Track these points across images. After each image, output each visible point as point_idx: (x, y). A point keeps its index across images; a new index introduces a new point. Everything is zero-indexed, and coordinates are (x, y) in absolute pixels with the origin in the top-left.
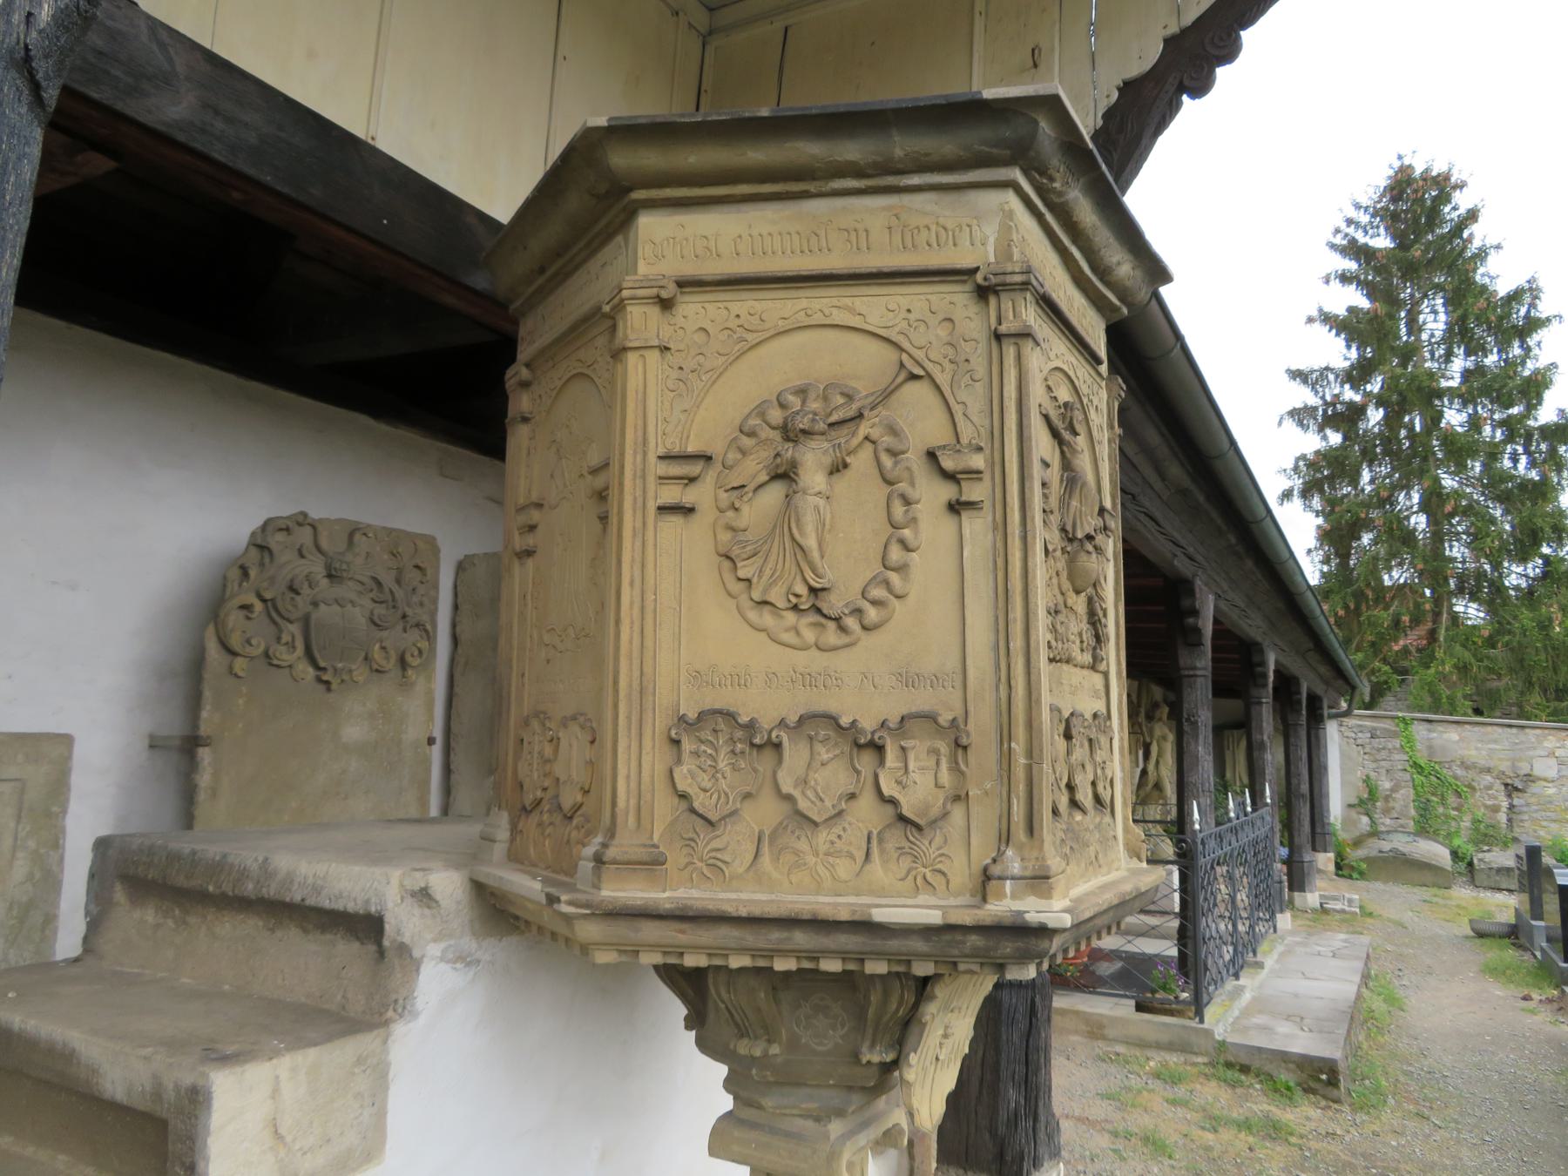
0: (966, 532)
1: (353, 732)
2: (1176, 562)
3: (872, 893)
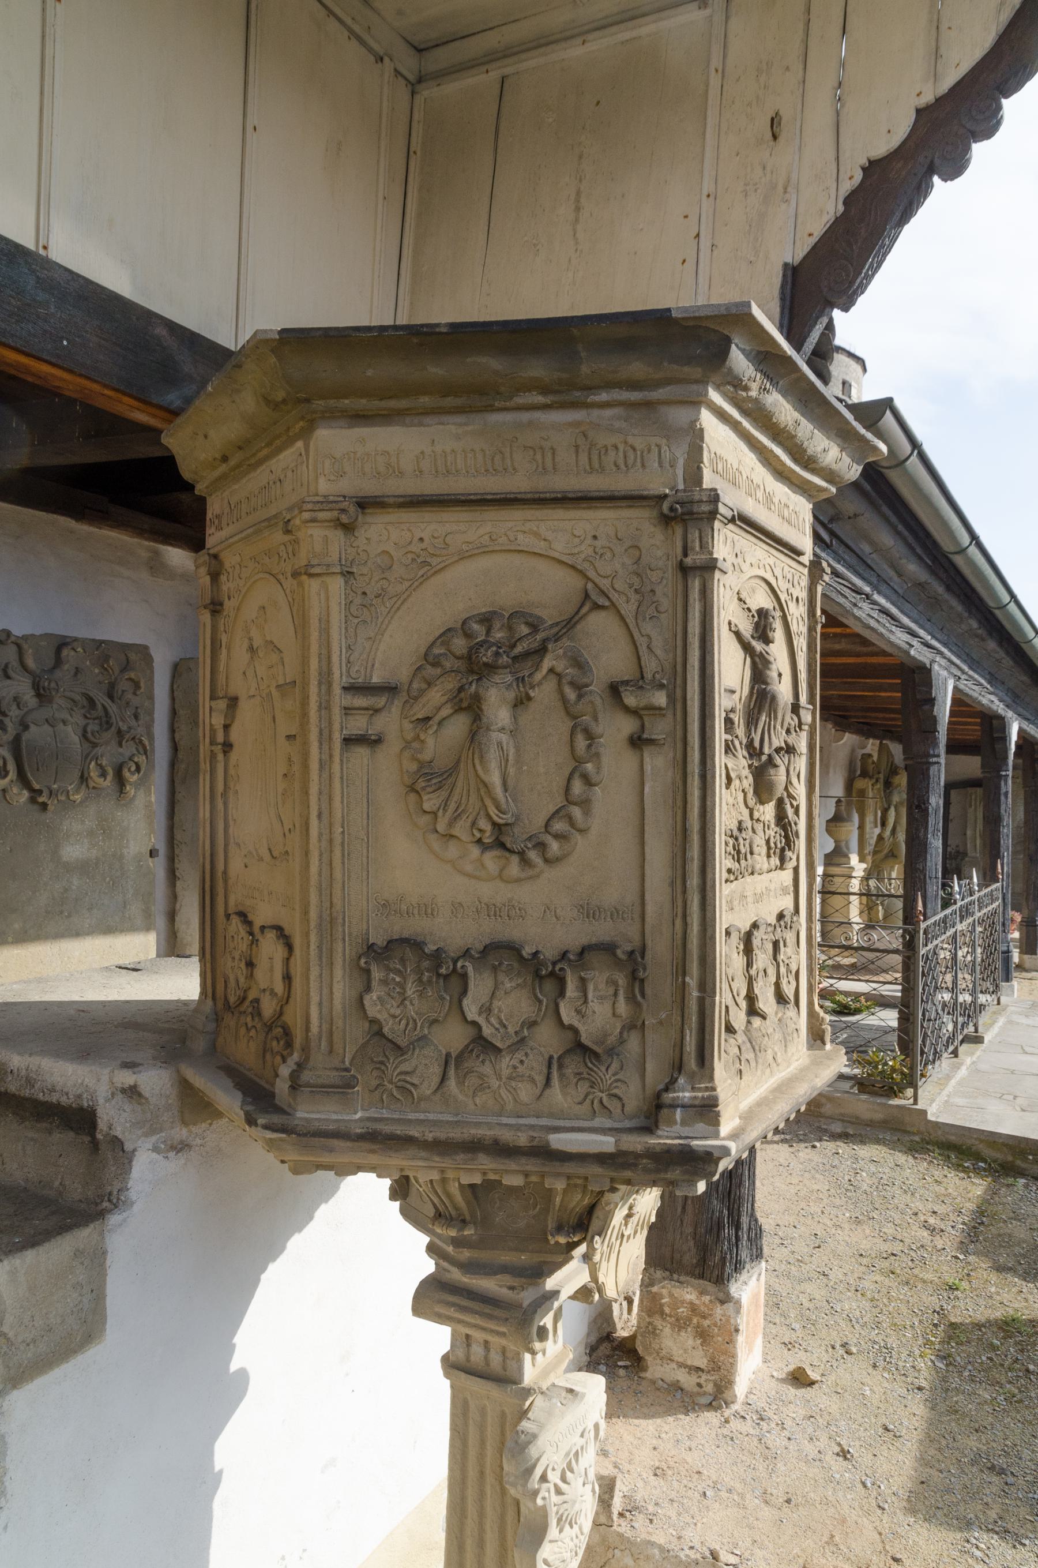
0: (648, 768)
1: (73, 851)
2: (912, 652)
3: (551, 1115)
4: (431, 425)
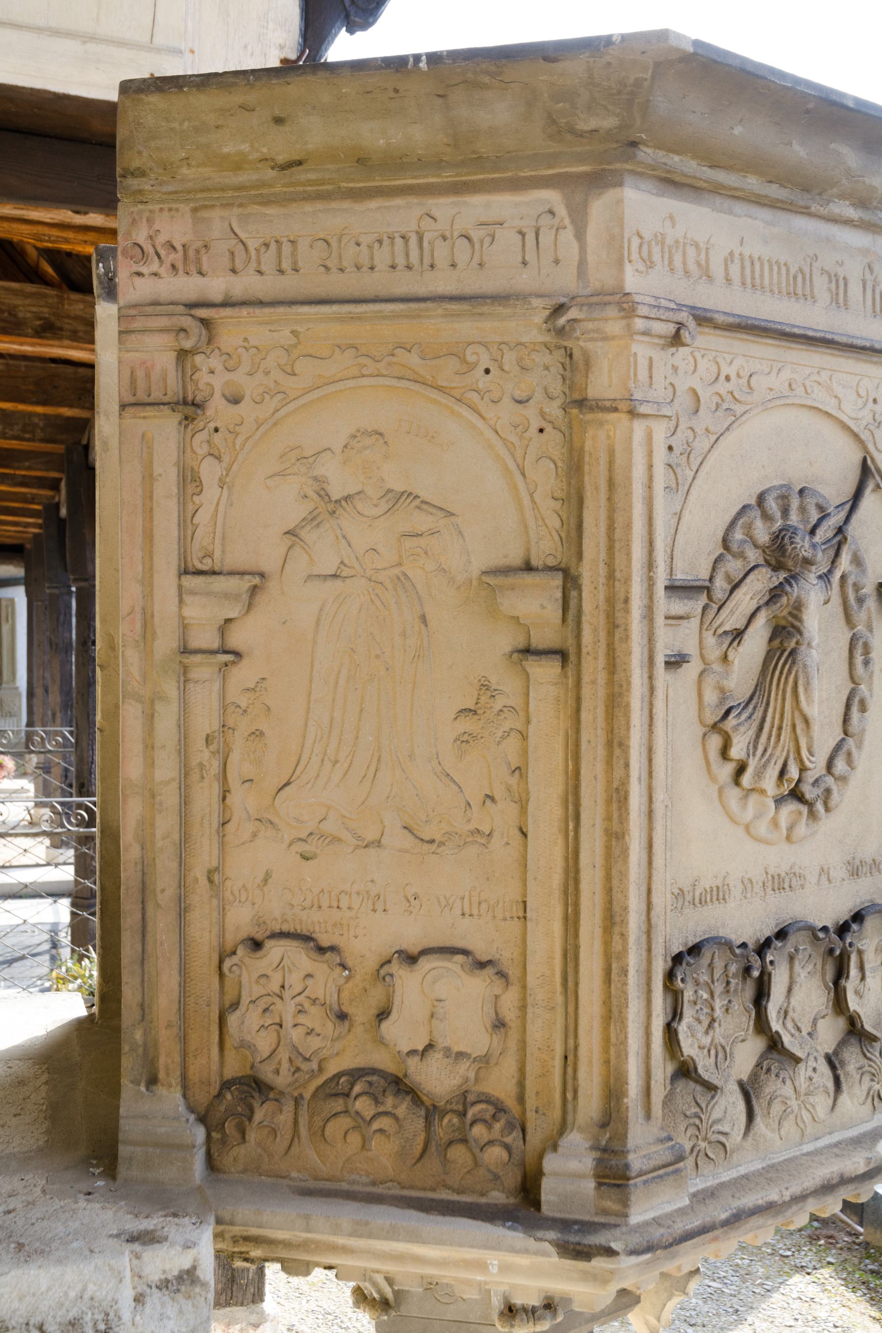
4: (739, 216)
